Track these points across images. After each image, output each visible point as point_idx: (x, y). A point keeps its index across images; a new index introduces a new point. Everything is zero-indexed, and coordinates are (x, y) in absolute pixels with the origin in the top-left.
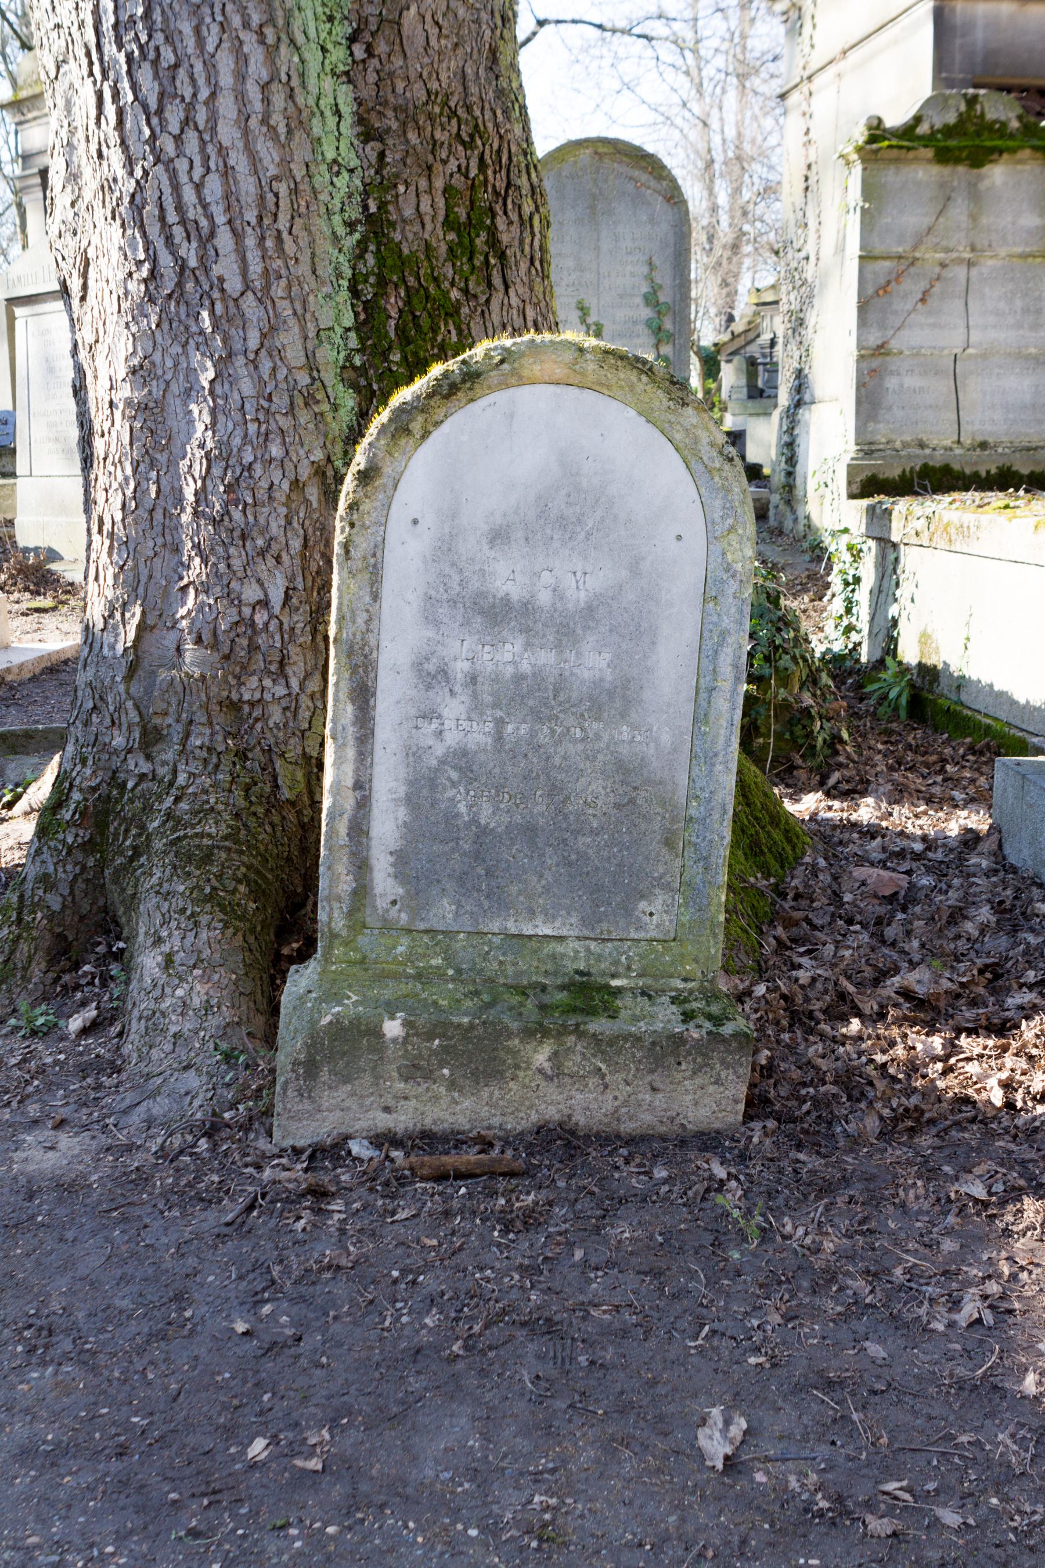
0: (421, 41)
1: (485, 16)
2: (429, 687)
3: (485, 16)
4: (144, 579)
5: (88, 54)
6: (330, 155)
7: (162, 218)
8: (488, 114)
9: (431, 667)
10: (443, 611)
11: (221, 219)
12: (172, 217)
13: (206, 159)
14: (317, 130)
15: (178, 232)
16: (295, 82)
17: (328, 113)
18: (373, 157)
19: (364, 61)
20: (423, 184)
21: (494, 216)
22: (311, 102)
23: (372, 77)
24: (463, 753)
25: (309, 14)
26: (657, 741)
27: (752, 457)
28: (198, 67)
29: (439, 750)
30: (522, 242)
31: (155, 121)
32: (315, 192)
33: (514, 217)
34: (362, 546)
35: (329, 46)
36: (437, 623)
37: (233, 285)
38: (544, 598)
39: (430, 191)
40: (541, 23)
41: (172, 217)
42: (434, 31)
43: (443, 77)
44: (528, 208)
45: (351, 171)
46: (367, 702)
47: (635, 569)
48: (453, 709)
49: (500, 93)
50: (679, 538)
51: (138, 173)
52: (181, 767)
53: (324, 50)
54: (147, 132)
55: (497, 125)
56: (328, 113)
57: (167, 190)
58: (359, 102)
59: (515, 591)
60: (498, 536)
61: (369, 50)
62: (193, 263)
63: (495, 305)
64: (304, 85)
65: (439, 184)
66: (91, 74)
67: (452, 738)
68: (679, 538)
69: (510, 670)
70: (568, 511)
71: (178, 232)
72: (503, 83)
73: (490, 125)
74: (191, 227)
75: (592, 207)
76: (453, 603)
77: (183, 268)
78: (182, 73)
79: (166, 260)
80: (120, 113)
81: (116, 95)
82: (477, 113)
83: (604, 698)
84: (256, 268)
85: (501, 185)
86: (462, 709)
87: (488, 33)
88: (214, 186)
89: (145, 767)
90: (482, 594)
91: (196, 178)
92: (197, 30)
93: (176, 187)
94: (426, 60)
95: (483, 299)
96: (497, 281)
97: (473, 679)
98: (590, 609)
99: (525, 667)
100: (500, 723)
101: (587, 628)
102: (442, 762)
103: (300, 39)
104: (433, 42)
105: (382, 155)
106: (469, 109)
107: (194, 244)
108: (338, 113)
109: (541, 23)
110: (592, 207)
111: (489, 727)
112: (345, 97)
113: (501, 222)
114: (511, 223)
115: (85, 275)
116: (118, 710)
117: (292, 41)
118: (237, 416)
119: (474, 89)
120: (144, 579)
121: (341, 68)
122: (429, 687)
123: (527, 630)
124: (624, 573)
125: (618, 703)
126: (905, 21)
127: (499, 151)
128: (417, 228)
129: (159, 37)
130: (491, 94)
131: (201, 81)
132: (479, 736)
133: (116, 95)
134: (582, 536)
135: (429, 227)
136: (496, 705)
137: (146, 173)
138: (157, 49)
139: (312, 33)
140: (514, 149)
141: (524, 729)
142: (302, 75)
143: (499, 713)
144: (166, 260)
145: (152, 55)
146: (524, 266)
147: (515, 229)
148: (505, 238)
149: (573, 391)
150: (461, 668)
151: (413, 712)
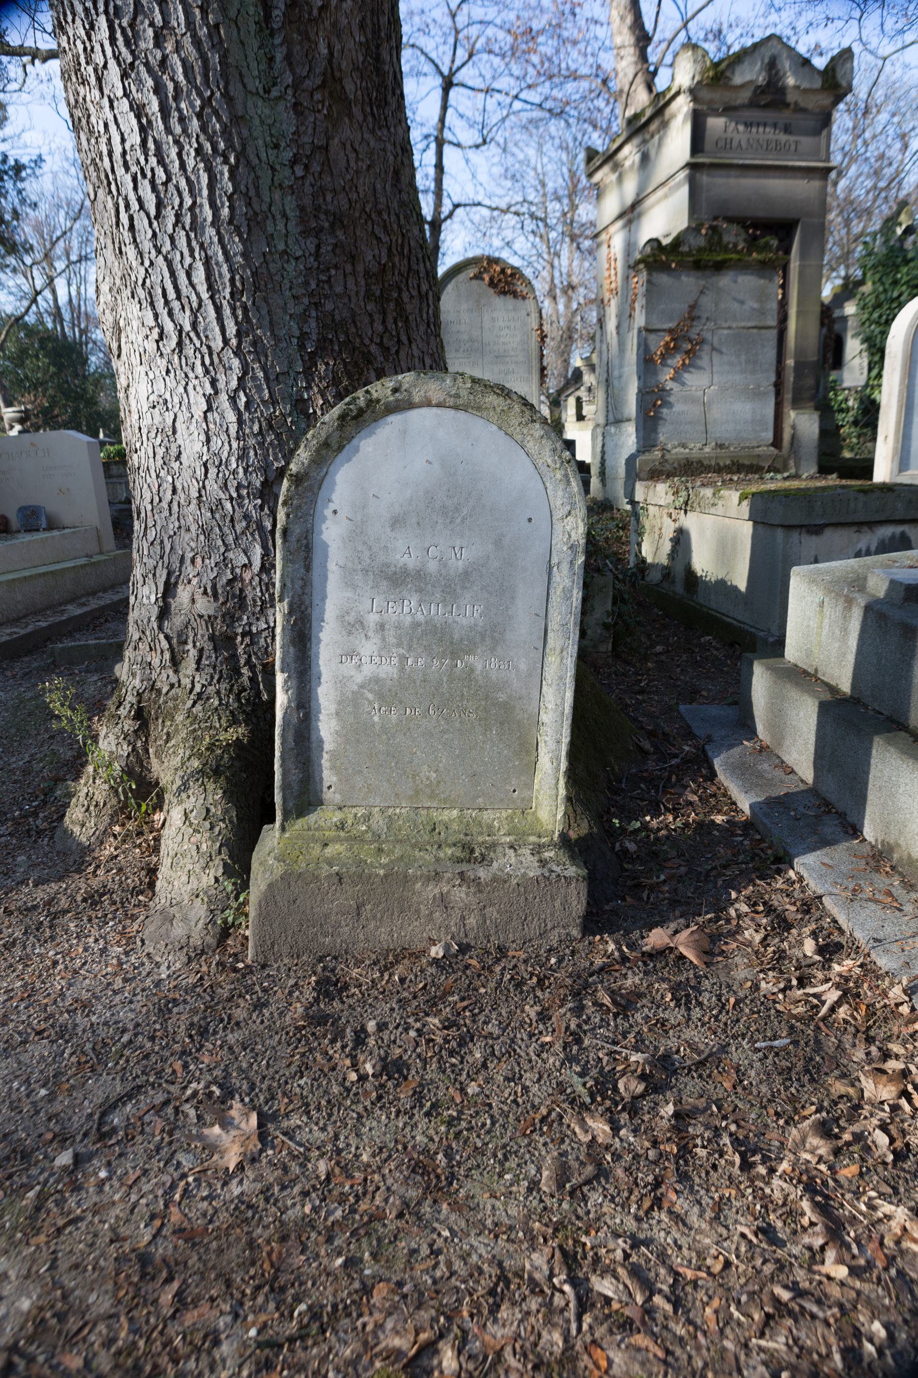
0: (344, 163)
1: (389, 147)
2: (350, 633)
3: (389, 147)
4: (167, 550)
5: (107, 177)
6: (281, 247)
7: (164, 295)
8: (393, 218)
9: (351, 618)
10: (359, 578)
11: (205, 296)
12: (172, 295)
13: (192, 251)
14: (270, 229)
15: (176, 305)
16: (252, 193)
17: (278, 217)
18: (312, 249)
19: (303, 178)
20: (349, 268)
21: (400, 291)
22: (265, 207)
23: (308, 190)
24: (376, 680)
25: (260, 142)
26: (516, 668)
27: (579, 457)
28: (183, 184)
29: (359, 679)
30: (421, 310)
31: (155, 224)
32: (271, 276)
33: (415, 293)
34: (297, 530)
35: (278, 167)
36: (354, 587)
37: (218, 344)
38: (432, 567)
39: (354, 273)
40: (456, 206)
41: (172, 295)
42: (352, 156)
43: (360, 190)
44: (424, 287)
45: (297, 259)
46: (305, 646)
47: (498, 543)
48: (368, 648)
49: (402, 204)
50: (530, 520)
51: (147, 263)
52: (197, 679)
53: (273, 169)
54: (150, 233)
55: (400, 226)
56: (278, 217)
57: (167, 274)
58: (302, 209)
59: (412, 562)
60: (396, 522)
61: (306, 167)
62: (187, 327)
63: (402, 355)
64: (258, 195)
65: (360, 268)
66: (110, 192)
67: (368, 670)
68: (530, 520)
69: (408, 620)
70: (452, 503)
71: (176, 305)
72: (405, 196)
73: (395, 227)
74: (185, 301)
75: (478, 301)
76: (365, 571)
77: (180, 332)
78: (171, 187)
79: (169, 326)
80: (131, 218)
81: (127, 207)
82: (385, 217)
83: (478, 639)
84: (231, 329)
85: (404, 270)
86: (375, 648)
87: (391, 158)
88: (199, 275)
89: (174, 679)
90: (388, 565)
91: (186, 266)
92: (179, 155)
93: (173, 274)
94: (348, 177)
95: (393, 350)
96: (404, 338)
97: (382, 627)
98: (466, 574)
99: (420, 617)
100: (403, 659)
101: (464, 588)
102: (362, 686)
103: (255, 161)
104: (352, 164)
105: (318, 247)
106: (379, 213)
107: (188, 313)
108: (284, 215)
109: (456, 206)
110: (478, 301)
111: (395, 661)
112: (290, 204)
113: (405, 296)
114: (412, 297)
115: (119, 340)
116: (153, 640)
117: (248, 163)
118: (224, 437)
119: (382, 200)
120: (167, 550)
121: (287, 183)
122: (350, 633)
123: (420, 590)
124: (491, 547)
125: (488, 641)
126: (672, 183)
127: (402, 246)
128: (346, 300)
129: (153, 161)
130: (395, 204)
131: (186, 194)
132: (388, 670)
133: (127, 207)
134: (459, 520)
135: (354, 300)
136: (399, 645)
137: (152, 263)
138: (152, 170)
139: (263, 156)
140: (412, 243)
141: (421, 661)
142: (257, 188)
143: (401, 651)
144: (169, 326)
145: (149, 175)
146: (422, 328)
147: (416, 301)
148: (408, 308)
149: (451, 413)
150: (372, 619)
151: (339, 652)
